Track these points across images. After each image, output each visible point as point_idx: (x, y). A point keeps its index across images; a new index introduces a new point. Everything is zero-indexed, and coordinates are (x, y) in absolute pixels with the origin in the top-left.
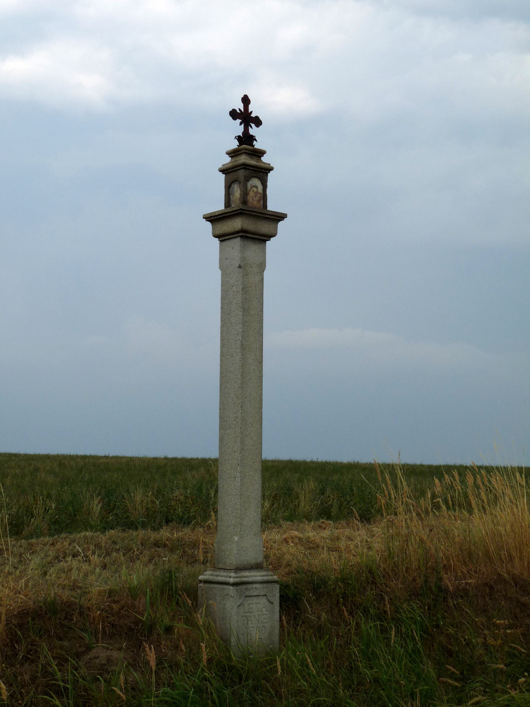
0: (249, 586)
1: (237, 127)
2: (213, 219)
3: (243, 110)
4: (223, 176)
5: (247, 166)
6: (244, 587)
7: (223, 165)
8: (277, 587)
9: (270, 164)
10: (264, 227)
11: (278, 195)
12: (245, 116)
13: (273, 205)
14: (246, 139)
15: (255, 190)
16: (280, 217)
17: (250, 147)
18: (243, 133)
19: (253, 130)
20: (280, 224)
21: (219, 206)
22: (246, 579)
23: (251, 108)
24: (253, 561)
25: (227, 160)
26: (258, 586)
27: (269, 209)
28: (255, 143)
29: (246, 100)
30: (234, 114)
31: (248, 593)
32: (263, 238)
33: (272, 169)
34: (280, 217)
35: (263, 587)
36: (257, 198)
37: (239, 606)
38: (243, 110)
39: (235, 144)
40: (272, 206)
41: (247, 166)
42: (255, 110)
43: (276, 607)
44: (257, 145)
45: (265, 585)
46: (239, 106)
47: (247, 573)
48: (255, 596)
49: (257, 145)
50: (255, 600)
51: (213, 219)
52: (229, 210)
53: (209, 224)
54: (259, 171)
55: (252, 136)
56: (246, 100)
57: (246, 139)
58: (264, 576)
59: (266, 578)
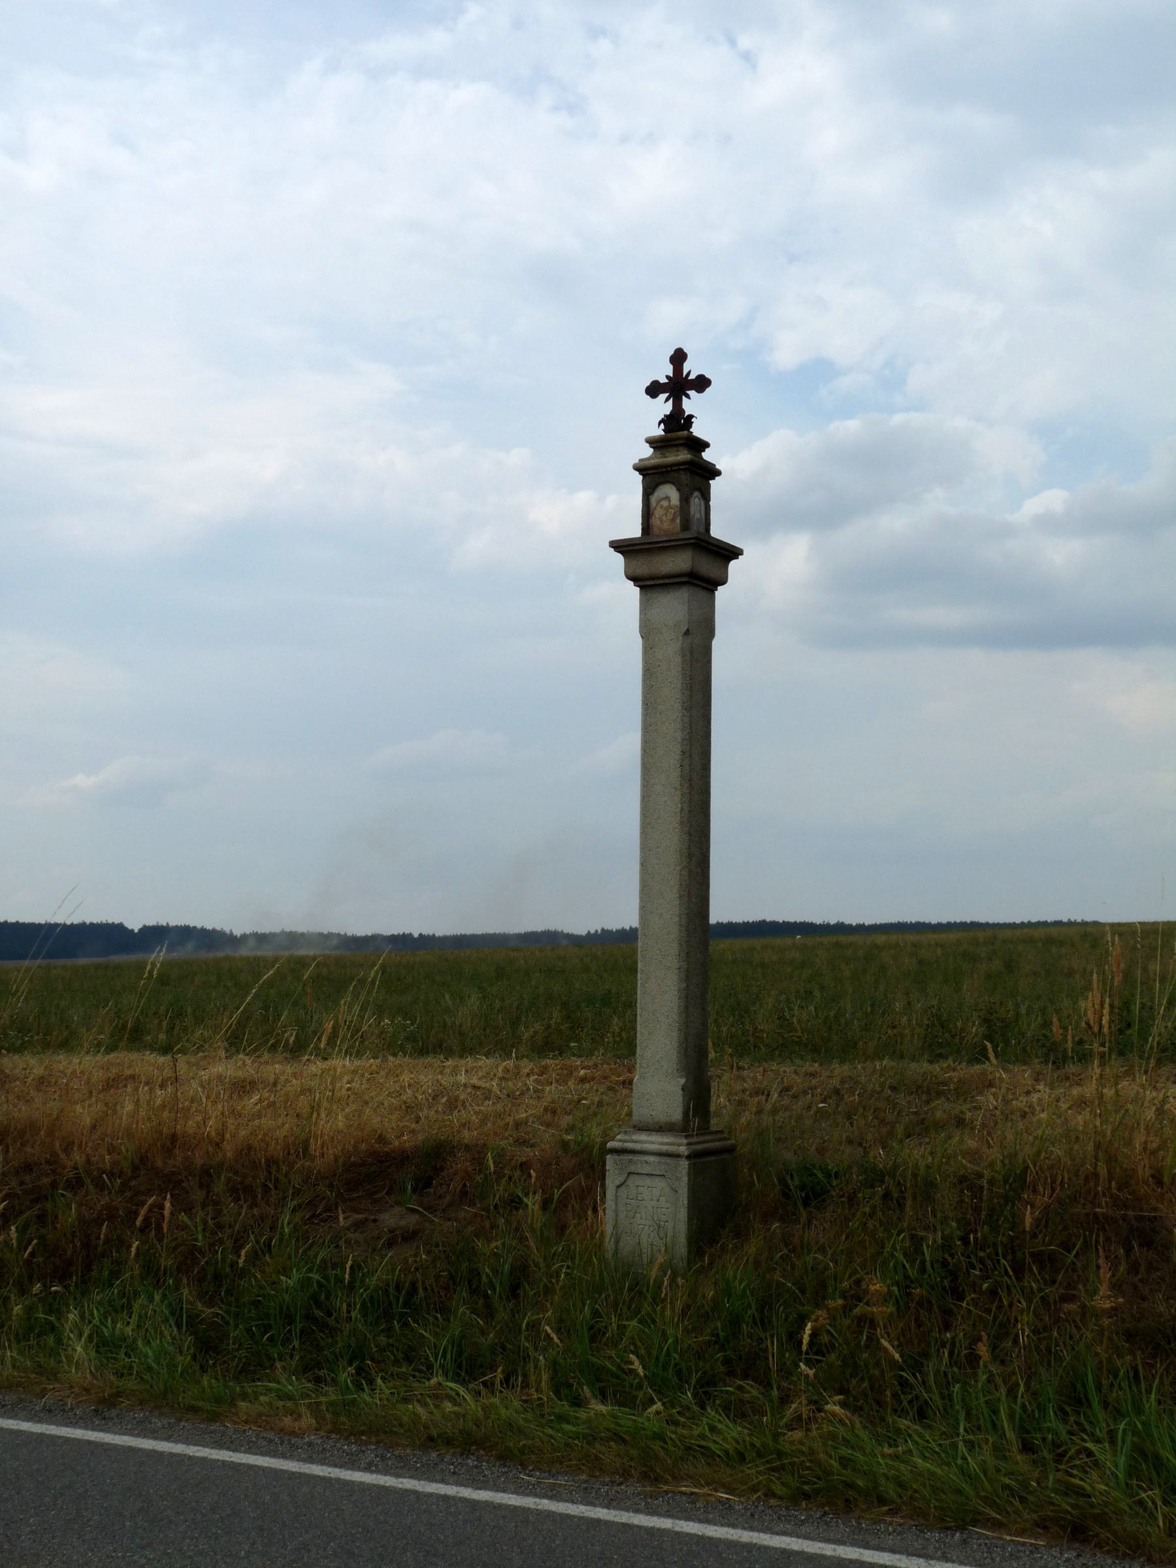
0: (636, 1158)
1: (662, 406)
2: (620, 546)
4: (638, 478)
5: (679, 464)
6: (626, 1157)
7: (641, 460)
8: (685, 1164)
10: (706, 567)
13: (719, 531)
14: (677, 422)
15: (665, 503)
19: (692, 404)
20: (733, 565)
21: (634, 530)
22: (630, 1145)
23: (687, 367)
24: (663, 1119)
25: (648, 451)
26: (652, 1159)
31: (633, 1169)
32: (711, 583)
33: (719, 473)
36: (670, 516)
39: (659, 431)
41: (679, 464)
45: (668, 1160)
46: (692, 368)
47: (643, 1137)
49: (697, 430)
50: (648, 1181)
51: (620, 546)
52: (687, 535)
53: (619, 559)
54: (667, 472)
56: (679, 357)
57: (677, 422)
58: (667, 1144)
59: (665, 1148)
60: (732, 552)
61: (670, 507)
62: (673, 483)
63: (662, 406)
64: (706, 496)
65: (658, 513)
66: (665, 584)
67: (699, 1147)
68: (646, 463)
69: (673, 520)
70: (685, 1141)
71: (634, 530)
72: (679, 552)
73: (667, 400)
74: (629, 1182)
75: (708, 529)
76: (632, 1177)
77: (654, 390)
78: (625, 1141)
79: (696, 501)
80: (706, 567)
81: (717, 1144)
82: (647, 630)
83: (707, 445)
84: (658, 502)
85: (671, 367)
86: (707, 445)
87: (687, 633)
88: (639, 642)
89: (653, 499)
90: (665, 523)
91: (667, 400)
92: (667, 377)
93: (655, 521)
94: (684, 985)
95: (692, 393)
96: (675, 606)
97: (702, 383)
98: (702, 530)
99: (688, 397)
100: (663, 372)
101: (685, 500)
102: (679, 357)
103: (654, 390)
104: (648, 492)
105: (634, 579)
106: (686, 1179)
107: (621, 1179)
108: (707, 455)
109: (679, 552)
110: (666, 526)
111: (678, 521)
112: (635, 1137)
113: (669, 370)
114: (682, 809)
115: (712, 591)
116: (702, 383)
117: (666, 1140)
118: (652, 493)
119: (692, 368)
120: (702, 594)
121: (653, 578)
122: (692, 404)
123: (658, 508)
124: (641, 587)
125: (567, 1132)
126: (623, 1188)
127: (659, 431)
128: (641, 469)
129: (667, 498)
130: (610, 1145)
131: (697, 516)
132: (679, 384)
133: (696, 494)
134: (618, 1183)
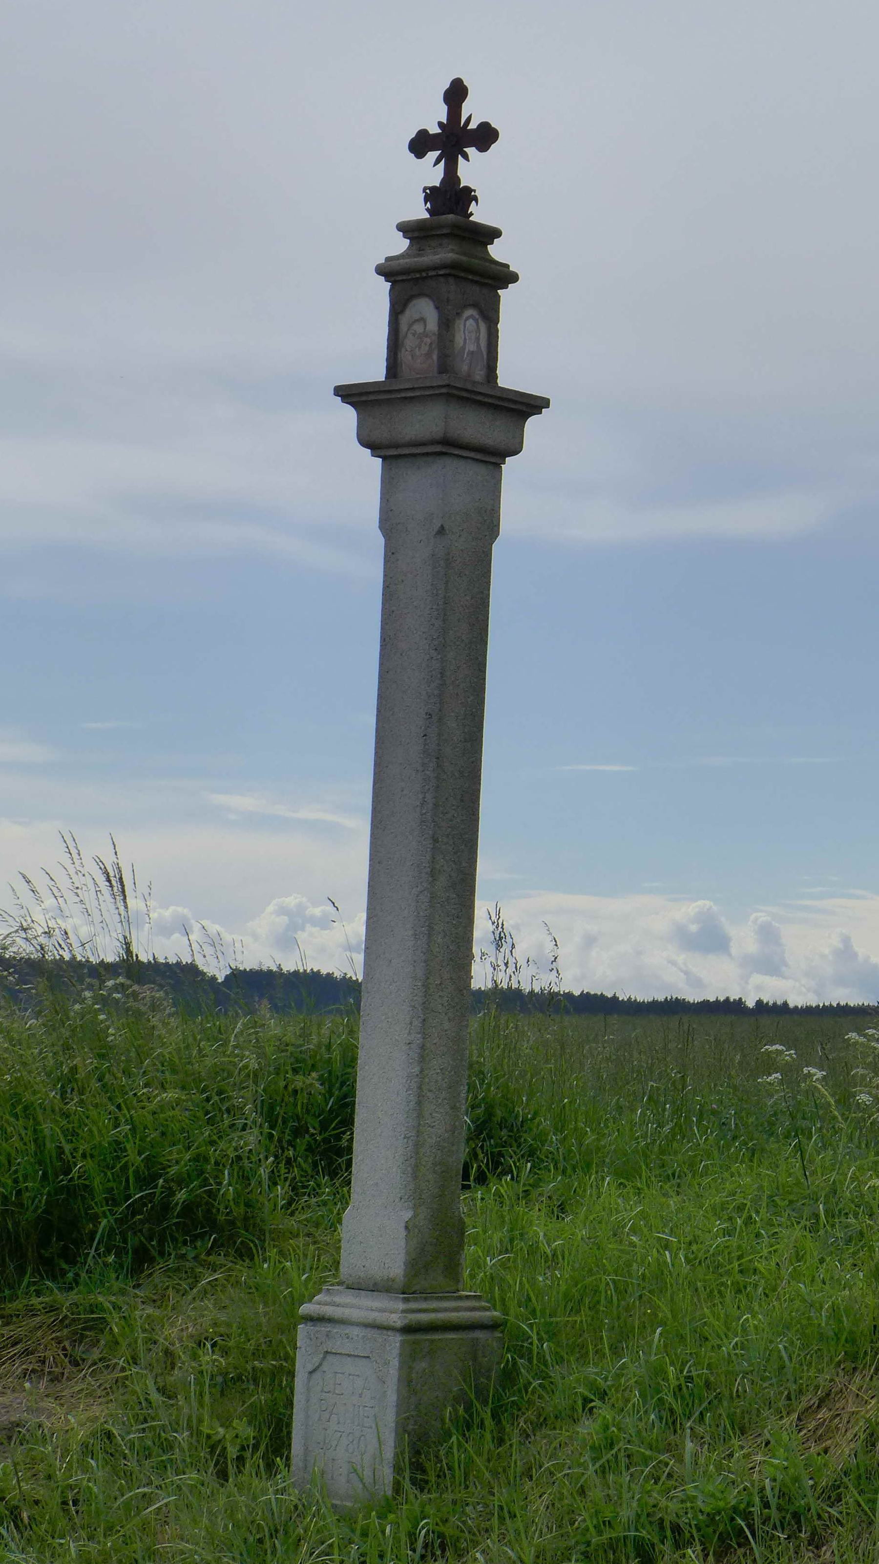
0: (336, 1330)
1: (430, 171)
2: (349, 394)
3: (438, 153)
5: (449, 265)
6: (323, 1328)
7: (388, 259)
9: (507, 266)
11: (525, 349)
14: (451, 198)
15: (418, 328)
16: (529, 406)
17: (460, 219)
19: (473, 169)
20: (532, 424)
21: (374, 371)
22: (329, 1311)
23: (467, 109)
25: (400, 245)
26: (355, 1331)
27: (502, 382)
28: (473, 208)
31: (329, 1346)
32: (493, 457)
33: (513, 278)
34: (529, 406)
35: (364, 1337)
36: (425, 349)
37: (311, 1373)
38: (438, 153)
39: (419, 211)
40: (509, 377)
41: (449, 265)
43: (389, 1393)
44: (479, 214)
46: (474, 111)
48: (349, 1355)
49: (479, 214)
51: (349, 394)
53: (349, 416)
55: (468, 190)
56: (456, 94)
57: (451, 198)
60: (528, 405)
61: (425, 334)
62: (437, 308)
63: (430, 171)
64: (490, 316)
65: (409, 342)
66: (414, 455)
67: (424, 1317)
68: (394, 263)
69: (428, 355)
70: (401, 1306)
71: (374, 371)
72: (442, 399)
73: (437, 162)
74: (325, 1367)
76: (330, 1358)
77: (420, 145)
78: (326, 1304)
79: (467, 328)
80: (473, 426)
81: (467, 1314)
82: (390, 522)
83: (495, 233)
84: (410, 325)
85: (445, 108)
86: (495, 233)
87: (441, 531)
88: (379, 541)
89: (404, 319)
90: (419, 359)
91: (437, 162)
92: (440, 124)
93: (405, 356)
94: (417, 1070)
95: (471, 151)
96: (437, 486)
97: (485, 136)
98: (479, 375)
99: (466, 157)
100: (433, 117)
101: (446, 324)
102: (456, 94)
103: (420, 145)
104: (398, 308)
105: (366, 442)
106: (395, 1363)
107: (316, 1360)
108: (497, 251)
109: (442, 399)
111: (435, 357)
112: (337, 1299)
113: (441, 113)
114: (424, 803)
115: (497, 466)
116: (485, 136)
117: (377, 1304)
118: (402, 311)
119: (474, 111)
120: (482, 470)
121: (397, 446)
122: (473, 169)
123: (410, 336)
124: (384, 458)
126: (317, 1375)
127: (419, 211)
128: (387, 271)
129: (422, 320)
130: (305, 1309)
131: (471, 347)
132: (455, 137)
133: (470, 312)
134: (310, 1367)
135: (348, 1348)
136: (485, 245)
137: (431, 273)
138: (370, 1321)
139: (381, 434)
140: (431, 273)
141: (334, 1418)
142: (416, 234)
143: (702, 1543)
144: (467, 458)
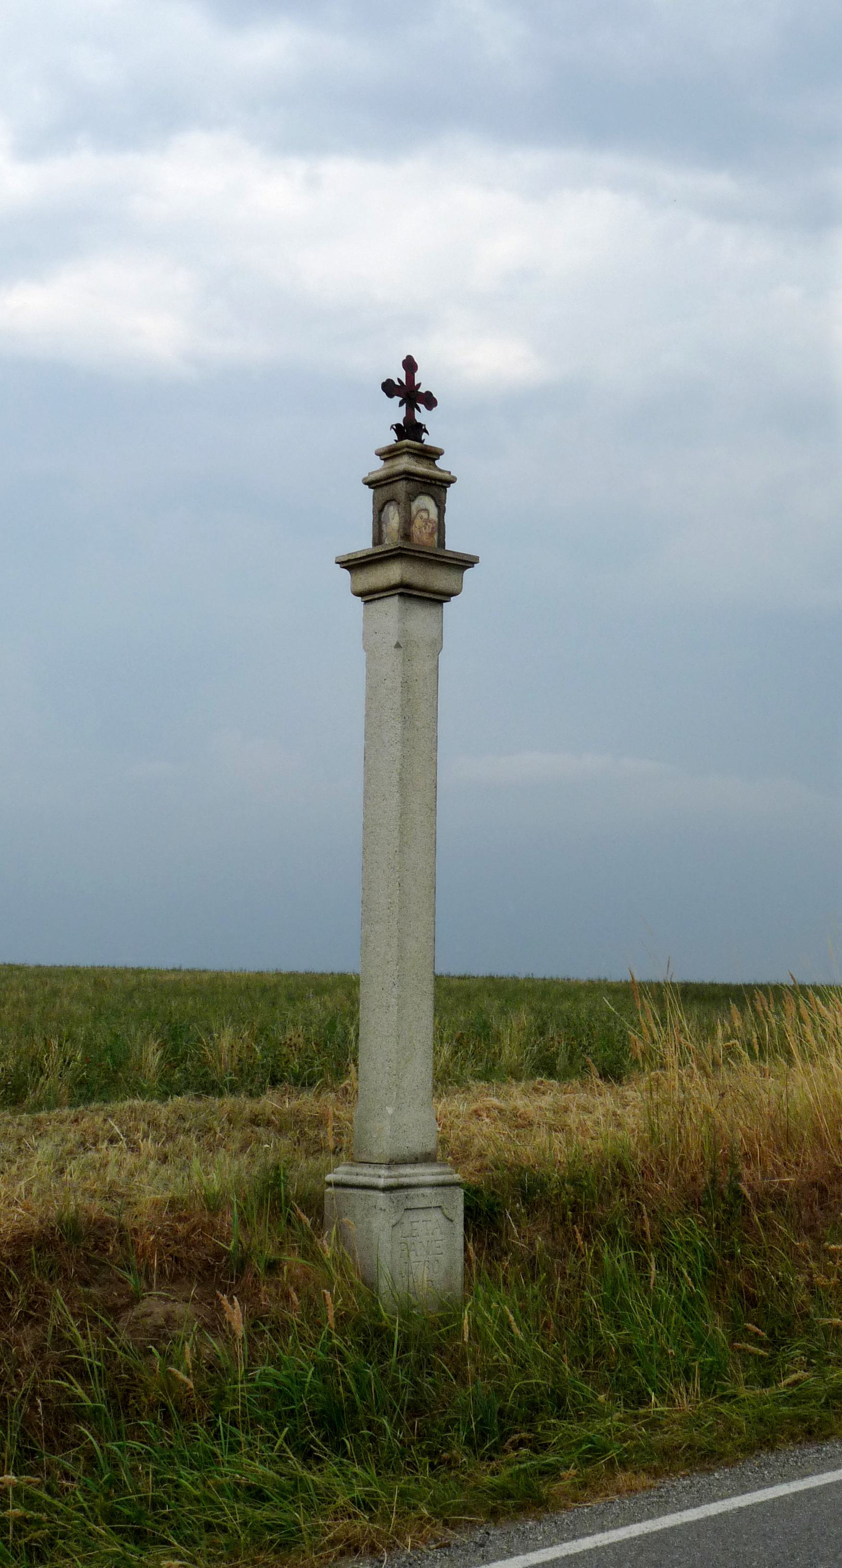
0: (412, 1192)
1: (395, 411)
5: (411, 474)
6: (403, 1193)
10: (439, 579)
12: (408, 392)
13: (455, 542)
14: (410, 430)
15: (425, 515)
16: (462, 563)
17: (418, 444)
18: (405, 420)
20: (468, 572)
21: (362, 542)
22: (406, 1181)
24: (418, 1149)
26: (427, 1191)
28: (424, 436)
29: (410, 365)
30: (389, 388)
31: (409, 1204)
33: (450, 482)
34: (462, 563)
36: (429, 530)
37: (393, 1226)
39: (390, 438)
41: (411, 474)
42: (424, 381)
44: (429, 440)
45: (440, 1190)
46: (399, 374)
47: (408, 1170)
49: (429, 440)
50: (422, 1215)
53: (346, 572)
54: (430, 484)
56: (410, 365)
57: (410, 430)
59: (441, 1178)
66: (383, 597)
75: (442, 543)
110: (425, 538)
125: (284, 1176)
135: (423, 1203)
136: (434, 460)
137: (438, 483)
138: (441, 1182)
139: (360, 588)
140: (438, 483)
141: (412, 1253)
142: (386, 456)
143: (565, 1273)
144: (383, 597)
